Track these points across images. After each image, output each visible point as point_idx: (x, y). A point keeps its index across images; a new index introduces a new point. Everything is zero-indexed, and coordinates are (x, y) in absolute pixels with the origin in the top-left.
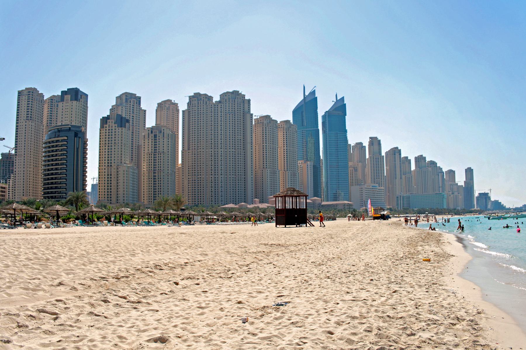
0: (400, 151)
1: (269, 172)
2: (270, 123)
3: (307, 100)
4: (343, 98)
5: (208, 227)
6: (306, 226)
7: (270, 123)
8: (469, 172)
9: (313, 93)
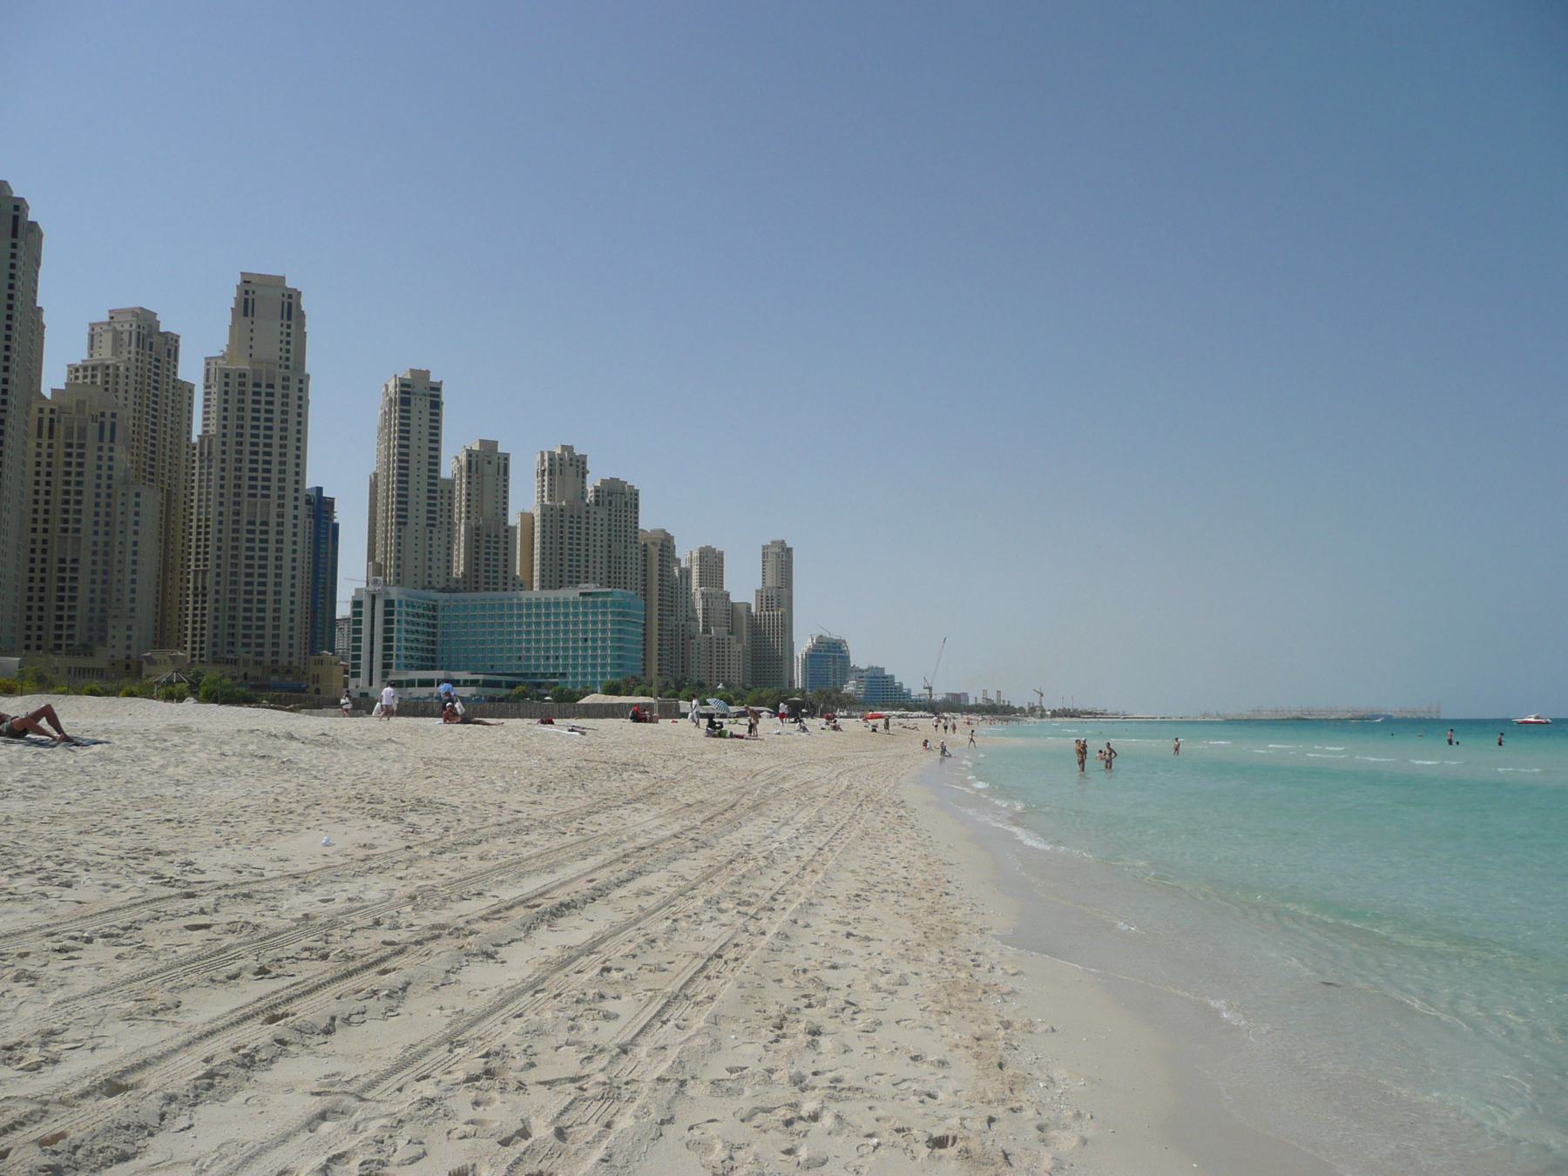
0: (436, 389)
8: (780, 560)
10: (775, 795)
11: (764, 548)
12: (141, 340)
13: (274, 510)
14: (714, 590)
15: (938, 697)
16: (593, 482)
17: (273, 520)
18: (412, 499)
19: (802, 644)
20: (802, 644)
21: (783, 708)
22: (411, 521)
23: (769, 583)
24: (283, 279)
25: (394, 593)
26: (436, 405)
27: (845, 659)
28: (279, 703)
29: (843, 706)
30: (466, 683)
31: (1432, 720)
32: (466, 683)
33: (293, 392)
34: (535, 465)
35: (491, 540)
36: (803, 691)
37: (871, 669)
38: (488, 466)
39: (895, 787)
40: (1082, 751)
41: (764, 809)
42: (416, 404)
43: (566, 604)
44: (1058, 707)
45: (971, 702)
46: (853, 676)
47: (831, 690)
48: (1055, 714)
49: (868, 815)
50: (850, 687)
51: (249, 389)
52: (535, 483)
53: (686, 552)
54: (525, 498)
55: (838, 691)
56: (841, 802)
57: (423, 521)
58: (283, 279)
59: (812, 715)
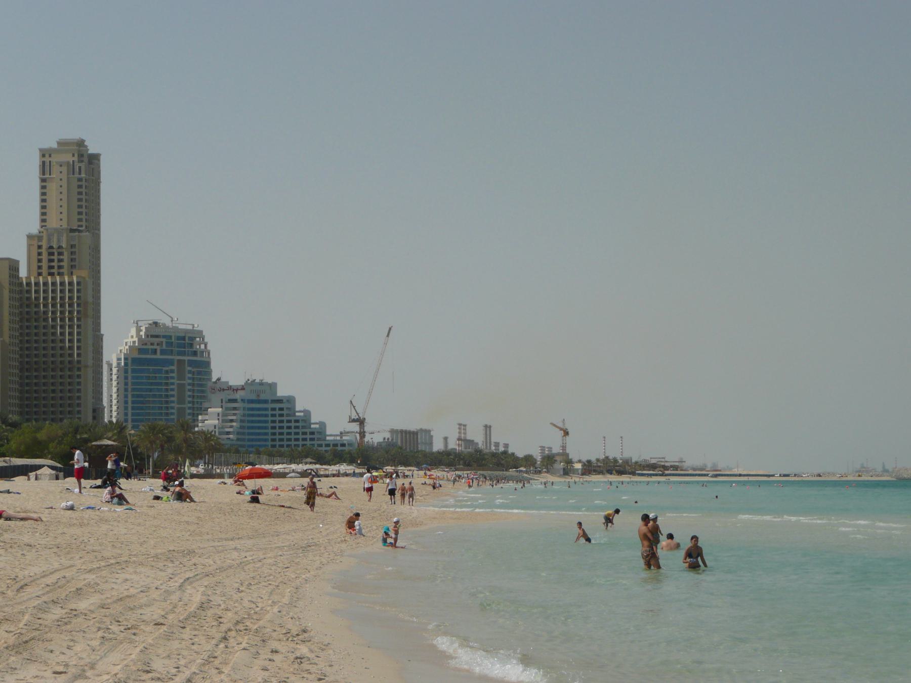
10: (61, 623)
11: (44, 153)
15: (376, 436)
19: (118, 338)
20: (118, 338)
21: (79, 459)
23: (54, 222)
27: (202, 366)
29: (195, 455)
36: (120, 428)
37: (250, 384)
39: (292, 604)
40: (651, 535)
41: (39, 649)
44: (594, 454)
45: (438, 446)
46: (216, 398)
47: (173, 425)
48: (590, 468)
49: (239, 657)
50: (210, 421)
55: (187, 427)
56: (187, 634)
59: (137, 470)
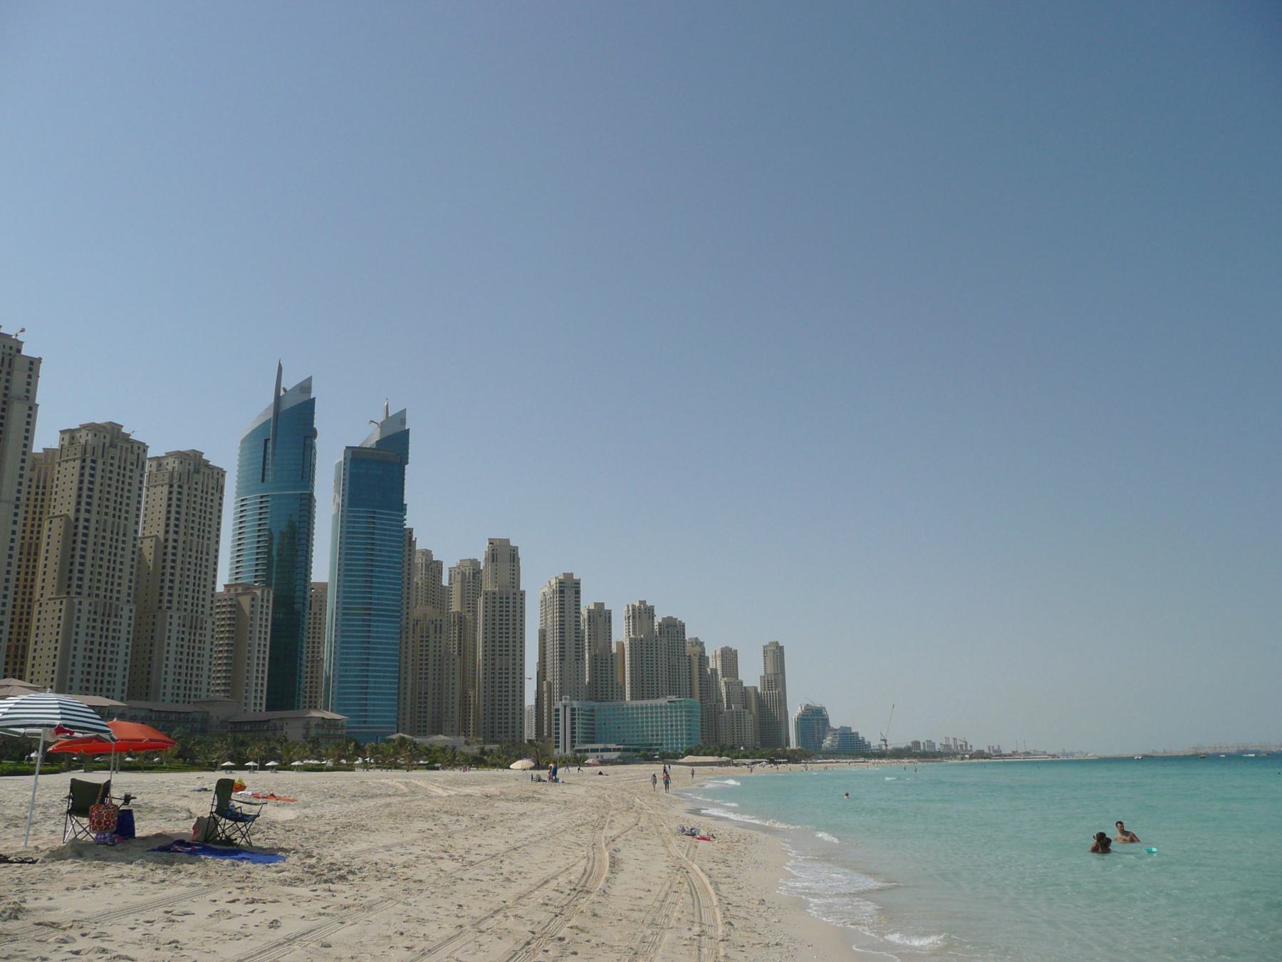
0: (577, 583)
1: (175, 621)
2: (113, 445)
3: (287, 405)
4: (310, 379)
5: (395, 777)
6: (955, 739)
7: (113, 445)
8: (776, 654)
9: (305, 387)
12: (427, 569)
13: (511, 661)
14: (733, 680)
16: (658, 620)
17: (511, 667)
18: (567, 645)
19: (794, 711)
20: (794, 711)
22: (567, 658)
24: (508, 541)
25: (575, 704)
26: (578, 592)
28: (387, 761)
30: (614, 750)
31: (915, 757)
32: (614, 750)
33: (518, 601)
34: (624, 614)
35: (605, 663)
38: (601, 617)
42: (568, 589)
43: (661, 707)
51: (498, 600)
52: (624, 624)
53: (712, 651)
54: (620, 633)
57: (573, 657)
58: (508, 541)
